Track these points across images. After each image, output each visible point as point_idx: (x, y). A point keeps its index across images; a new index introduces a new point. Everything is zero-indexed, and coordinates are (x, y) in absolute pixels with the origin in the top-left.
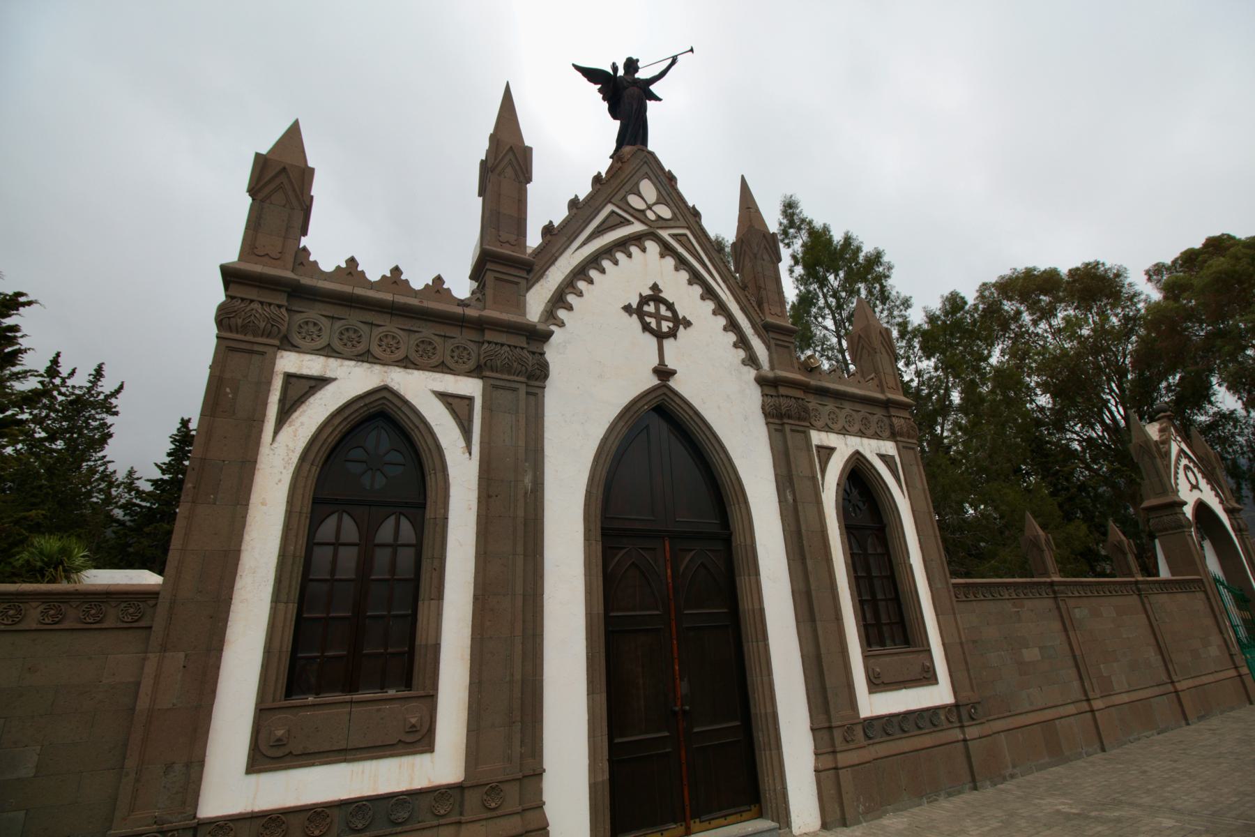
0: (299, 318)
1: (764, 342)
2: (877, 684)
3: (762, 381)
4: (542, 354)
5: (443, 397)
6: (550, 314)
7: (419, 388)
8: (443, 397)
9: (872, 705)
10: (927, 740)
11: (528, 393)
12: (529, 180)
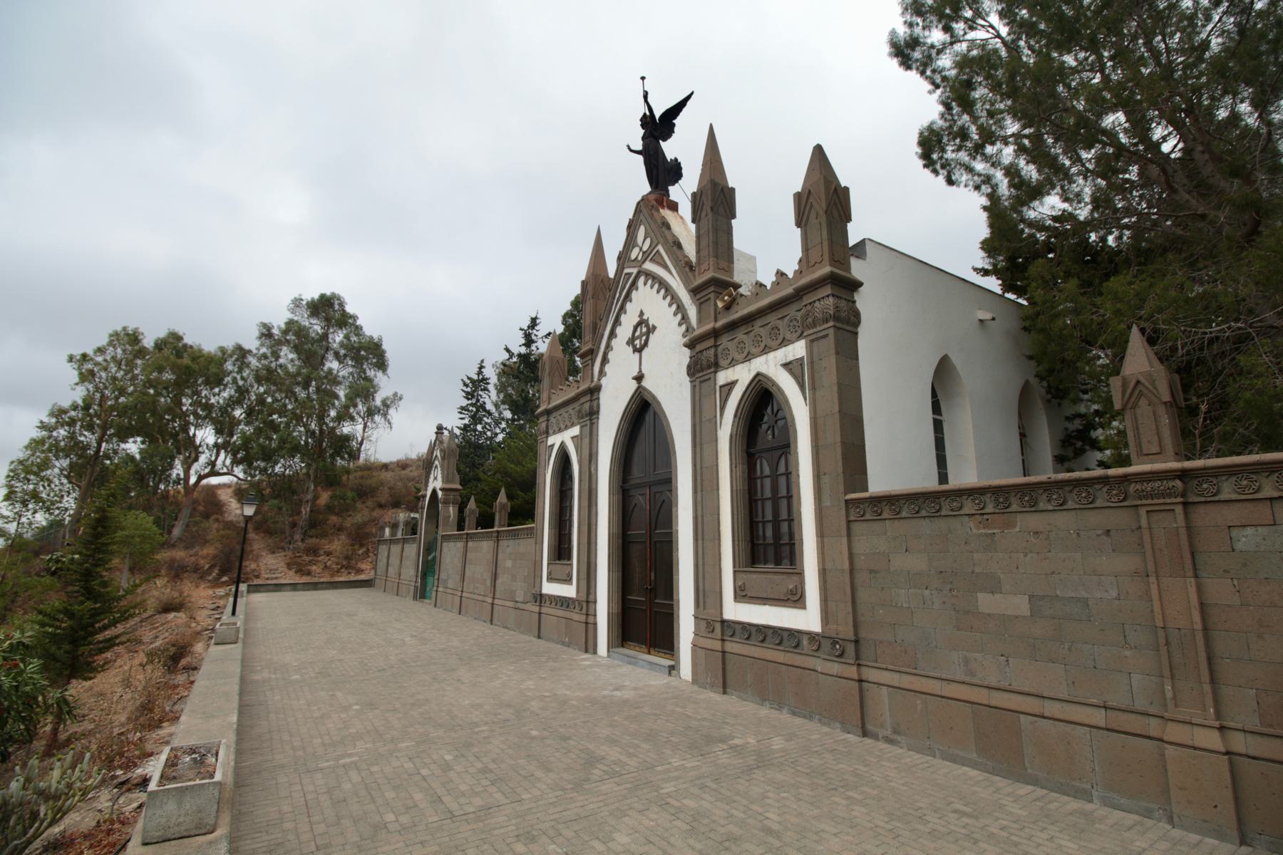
0: (720, 349)
1: (806, 248)
2: (742, 595)
5: (786, 366)
7: (771, 365)
8: (786, 366)
9: (735, 611)
10: (779, 656)
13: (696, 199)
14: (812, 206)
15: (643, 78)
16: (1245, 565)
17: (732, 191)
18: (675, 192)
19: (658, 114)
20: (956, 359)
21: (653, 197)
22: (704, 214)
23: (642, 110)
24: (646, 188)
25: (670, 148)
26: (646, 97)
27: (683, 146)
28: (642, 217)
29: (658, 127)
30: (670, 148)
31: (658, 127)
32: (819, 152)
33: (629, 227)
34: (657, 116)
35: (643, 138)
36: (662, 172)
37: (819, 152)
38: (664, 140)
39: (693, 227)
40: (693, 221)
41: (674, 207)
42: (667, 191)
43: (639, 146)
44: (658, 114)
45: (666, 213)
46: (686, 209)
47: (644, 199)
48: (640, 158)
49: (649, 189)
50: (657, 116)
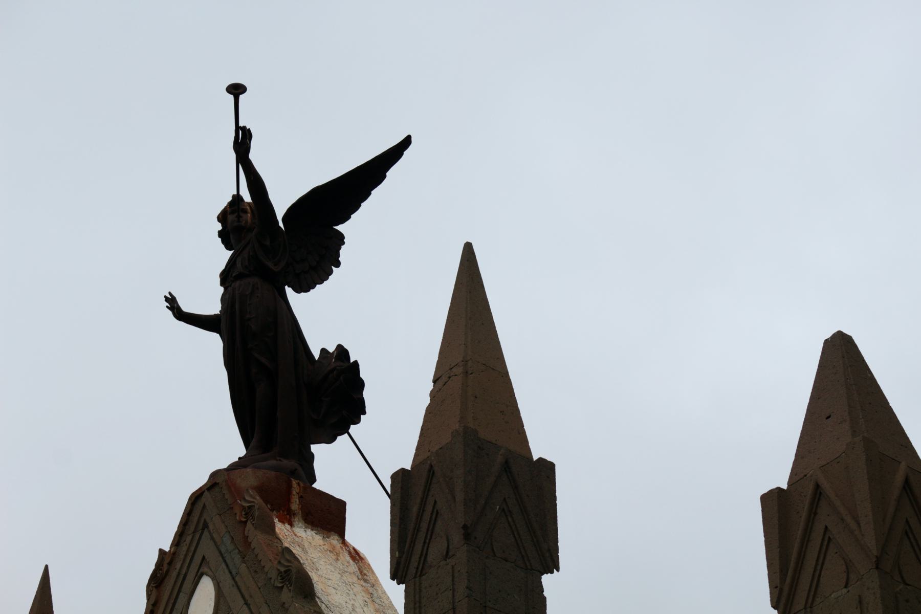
13: (408, 493)
14: (827, 540)
15: (236, 90)
16: (256, 572)
17: (545, 471)
18: (335, 466)
19: (282, 201)
20: (826, 485)
21: (249, 479)
22: (436, 550)
23: (225, 185)
24: (227, 446)
25: (321, 316)
26: (242, 142)
27: (373, 312)
28: (206, 548)
29: (279, 245)
30: (321, 316)
31: (279, 245)
32: (841, 356)
33: (156, 582)
34: (280, 211)
35: (226, 278)
36: (290, 394)
37: (841, 356)
38: (303, 287)
39: (396, 593)
40: (397, 574)
41: (329, 516)
42: (310, 458)
43: (208, 299)
44: (282, 201)
45: (302, 541)
46: (370, 527)
47: (218, 480)
48: (212, 344)
49: (241, 451)
50: (280, 211)
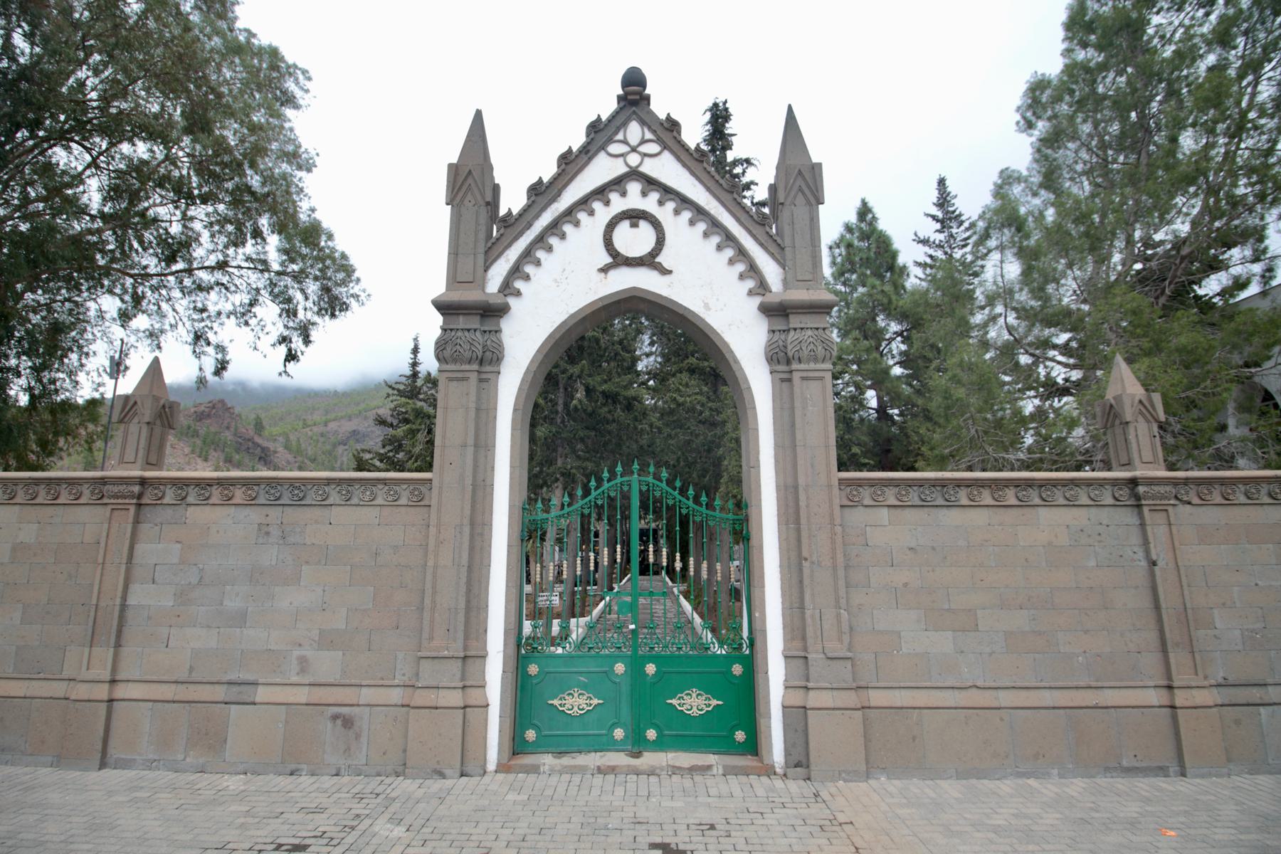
3: (766, 310)
4: (498, 331)
6: (507, 287)
11: (481, 380)
12: (820, 201)
